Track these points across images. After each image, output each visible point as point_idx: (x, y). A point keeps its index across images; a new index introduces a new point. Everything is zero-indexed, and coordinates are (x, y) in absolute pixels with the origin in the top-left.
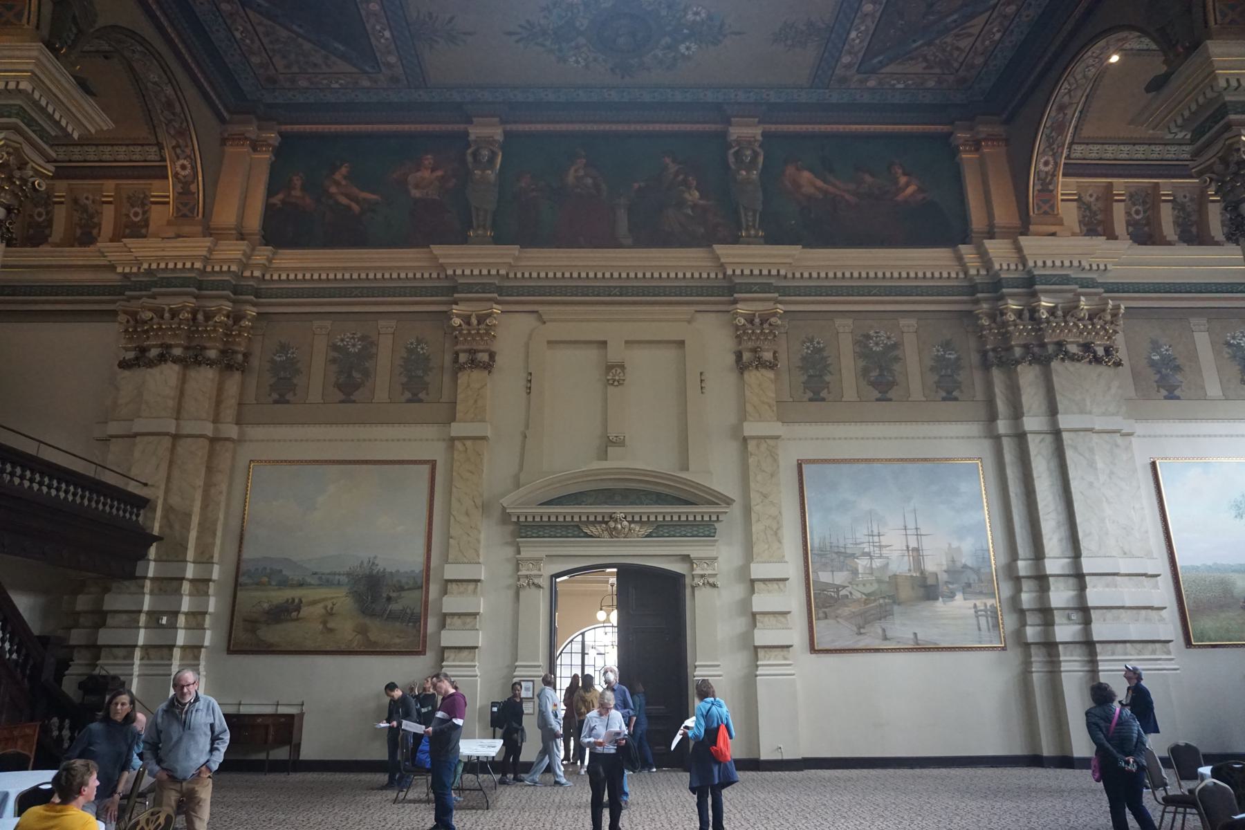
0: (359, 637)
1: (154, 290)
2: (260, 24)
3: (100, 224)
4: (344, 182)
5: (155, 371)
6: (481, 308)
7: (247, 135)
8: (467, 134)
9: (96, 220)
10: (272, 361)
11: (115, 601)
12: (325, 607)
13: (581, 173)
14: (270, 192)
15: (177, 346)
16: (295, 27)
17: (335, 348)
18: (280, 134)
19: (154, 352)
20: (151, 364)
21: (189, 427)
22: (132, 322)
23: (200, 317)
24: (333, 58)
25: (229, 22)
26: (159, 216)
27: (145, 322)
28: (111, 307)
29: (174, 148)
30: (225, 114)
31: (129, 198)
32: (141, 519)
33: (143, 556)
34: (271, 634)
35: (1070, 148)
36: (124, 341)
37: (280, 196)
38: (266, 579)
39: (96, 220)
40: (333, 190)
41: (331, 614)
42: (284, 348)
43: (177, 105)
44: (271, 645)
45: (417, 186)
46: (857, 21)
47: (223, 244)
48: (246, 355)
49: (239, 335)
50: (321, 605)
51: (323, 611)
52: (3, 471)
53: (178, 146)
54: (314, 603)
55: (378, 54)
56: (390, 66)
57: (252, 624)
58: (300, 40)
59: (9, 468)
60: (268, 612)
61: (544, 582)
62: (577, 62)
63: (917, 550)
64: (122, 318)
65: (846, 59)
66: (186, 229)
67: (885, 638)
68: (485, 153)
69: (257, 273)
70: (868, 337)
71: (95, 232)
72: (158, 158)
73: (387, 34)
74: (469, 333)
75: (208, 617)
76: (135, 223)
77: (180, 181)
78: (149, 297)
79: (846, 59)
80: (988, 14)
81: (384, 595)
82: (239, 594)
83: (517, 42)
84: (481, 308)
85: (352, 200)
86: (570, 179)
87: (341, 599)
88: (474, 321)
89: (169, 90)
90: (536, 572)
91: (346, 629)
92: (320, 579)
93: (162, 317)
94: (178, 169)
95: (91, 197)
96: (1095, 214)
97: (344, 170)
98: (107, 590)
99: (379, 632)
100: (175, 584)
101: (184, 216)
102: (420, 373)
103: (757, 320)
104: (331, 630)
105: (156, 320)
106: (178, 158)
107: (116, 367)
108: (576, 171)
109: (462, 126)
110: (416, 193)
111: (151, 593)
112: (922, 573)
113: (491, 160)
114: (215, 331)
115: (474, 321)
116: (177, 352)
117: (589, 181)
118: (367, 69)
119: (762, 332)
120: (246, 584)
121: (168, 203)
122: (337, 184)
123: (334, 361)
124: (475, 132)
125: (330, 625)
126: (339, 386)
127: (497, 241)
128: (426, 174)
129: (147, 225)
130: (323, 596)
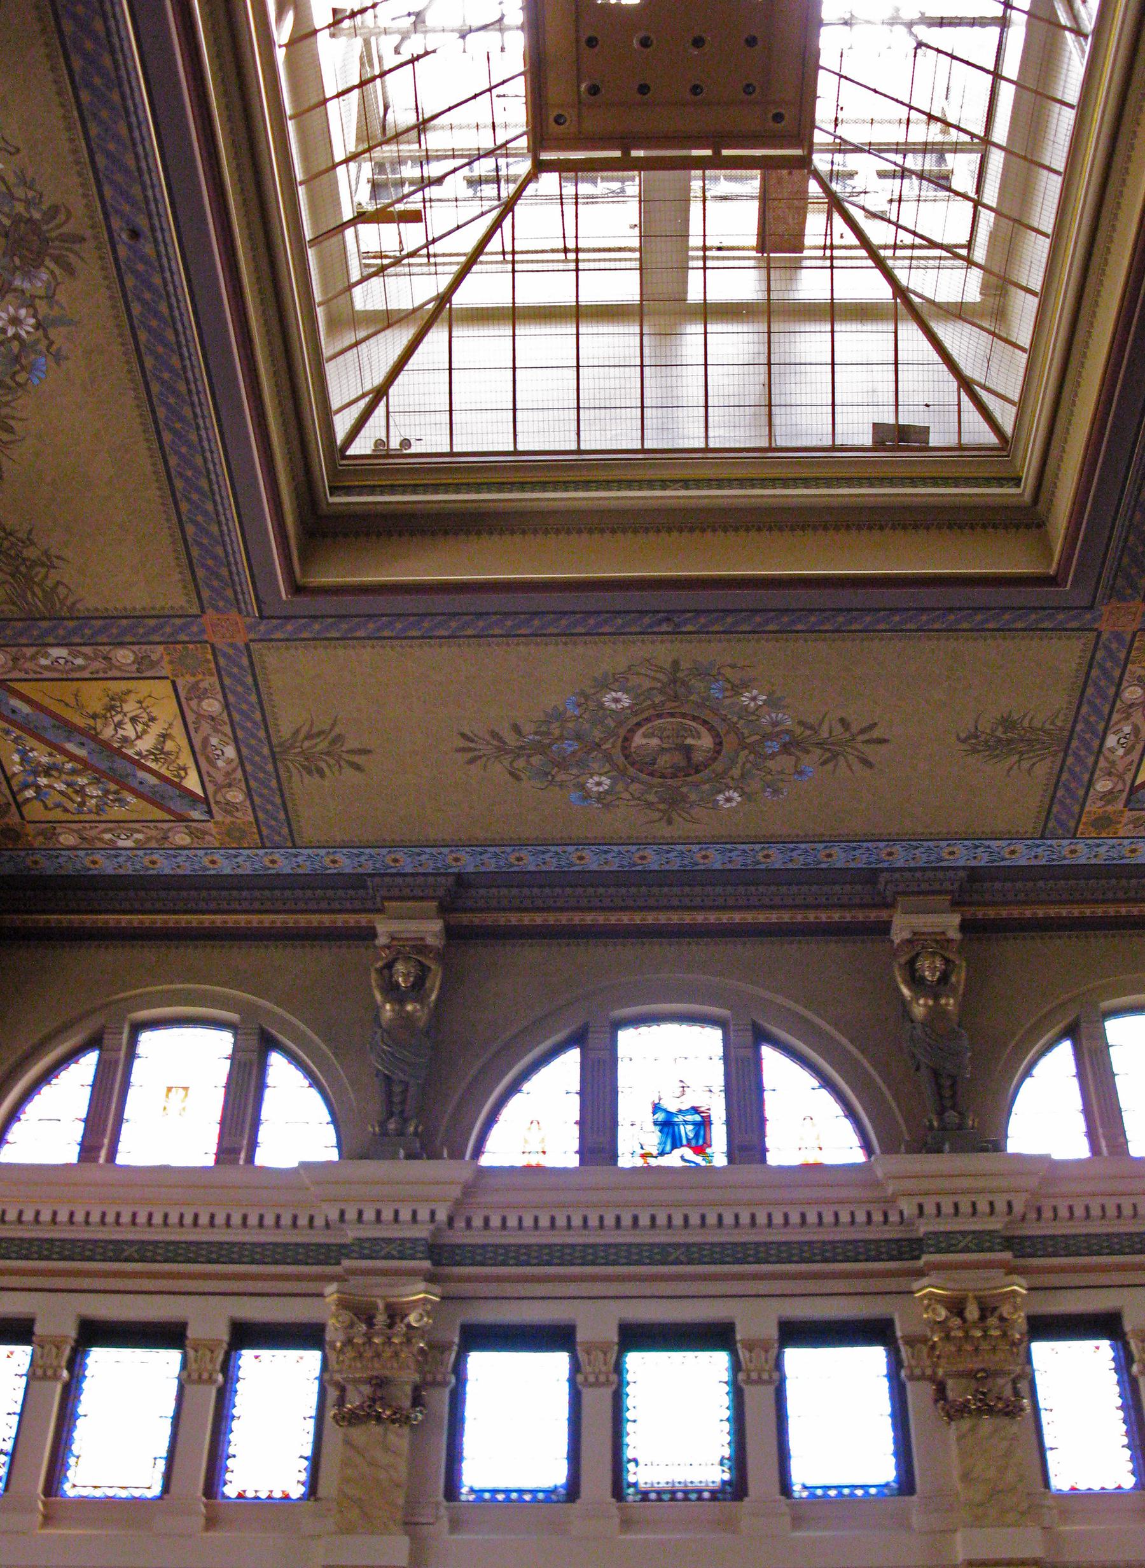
1: (346, 1263)
46: (1116, 717)
56: (230, 808)
65: (1103, 785)
73: (230, 752)
74: (967, 1337)
79: (1103, 785)
80: (11, 684)
115: (972, 1312)
119: (985, 1336)
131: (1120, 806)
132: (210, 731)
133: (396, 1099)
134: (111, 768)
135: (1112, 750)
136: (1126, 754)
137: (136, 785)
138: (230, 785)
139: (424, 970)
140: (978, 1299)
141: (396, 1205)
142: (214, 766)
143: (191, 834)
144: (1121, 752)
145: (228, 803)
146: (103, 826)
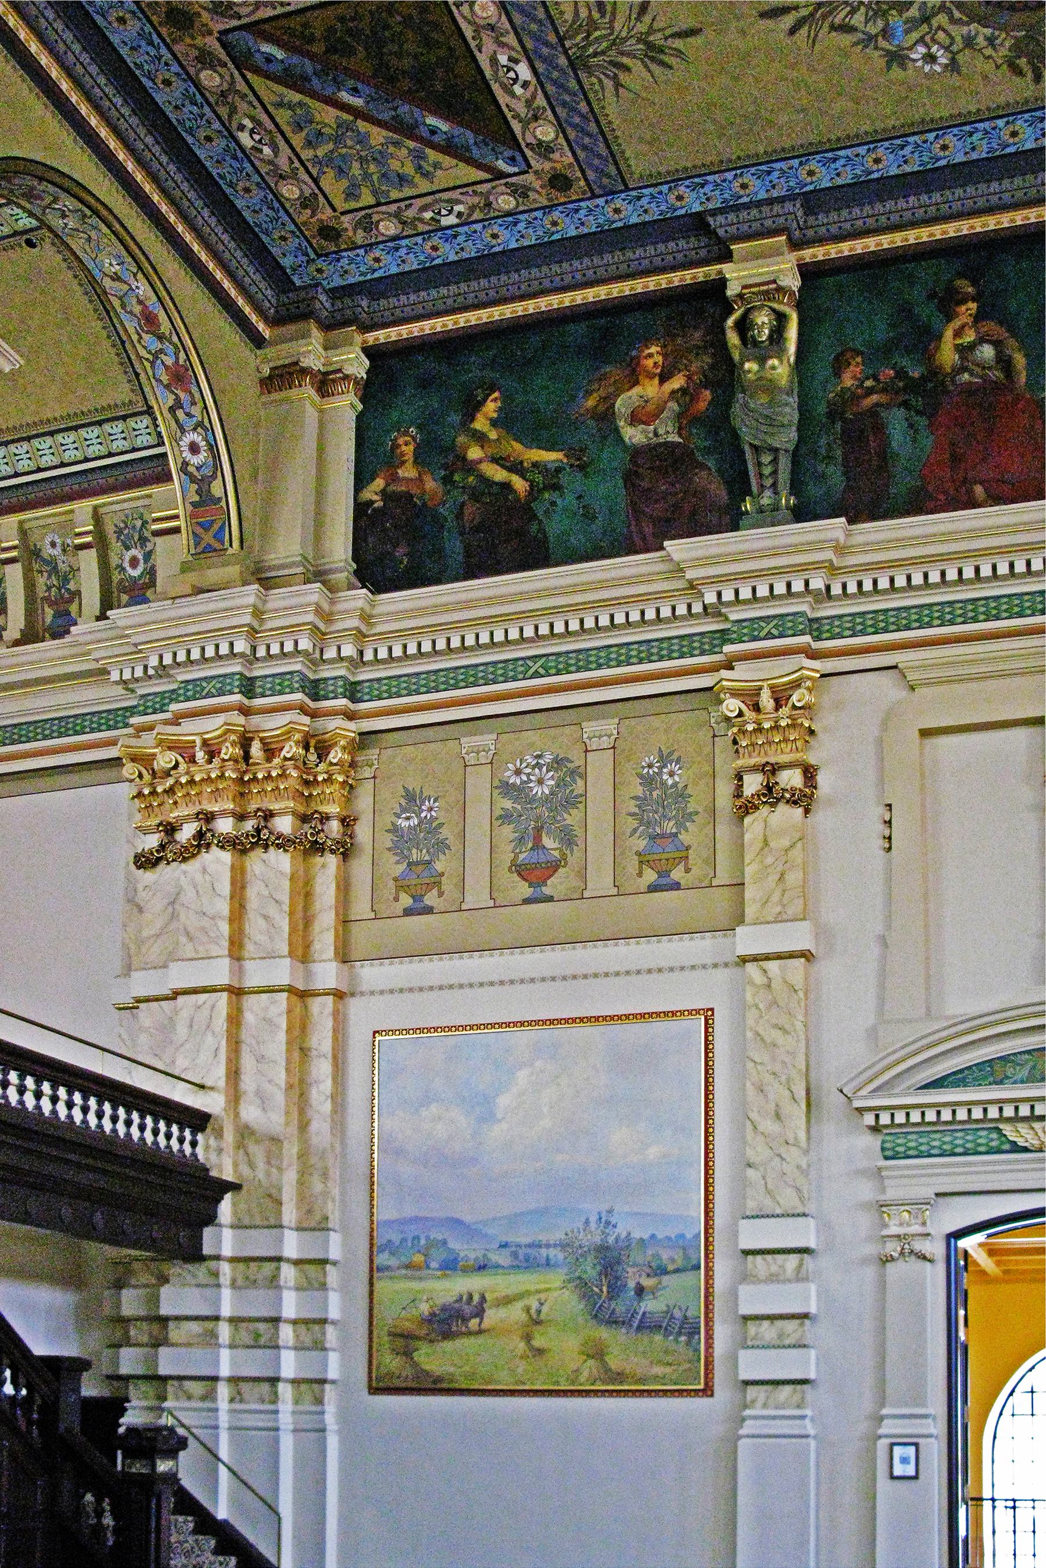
0: (591, 1362)
2: (280, 105)
3: (78, 593)
4: (493, 435)
5: (192, 867)
6: (779, 671)
7: (305, 363)
8: (722, 283)
9: (72, 586)
10: (395, 830)
11: (174, 1300)
12: (528, 1310)
13: (970, 337)
14: (361, 481)
15: (223, 813)
16: (345, 96)
17: (506, 789)
18: (367, 351)
19: (186, 833)
20: (186, 855)
21: (255, 975)
22: (147, 777)
23: (256, 750)
24: (432, 155)
25: (223, 111)
26: (170, 554)
27: (167, 774)
28: (112, 753)
29: (172, 410)
30: (261, 327)
31: (119, 532)
32: (199, 1150)
33: (210, 1219)
34: (434, 1358)
36: (138, 816)
37: (379, 483)
38: (419, 1258)
39: (72, 586)
40: (474, 453)
41: (538, 1323)
42: (412, 800)
43: (162, 316)
44: (439, 1379)
45: (635, 419)
47: (278, 598)
48: (347, 822)
49: (329, 780)
50: (520, 1305)
51: (524, 1317)
52: (5, 1084)
53: (178, 404)
54: (507, 1301)
55: (516, 127)
56: (544, 149)
57: (405, 1341)
58: (362, 126)
59: (13, 1077)
60: (430, 1319)
61: (936, 1248)
62: (931, 58)
64: (129, 769)
66: (214, 575)
68: (763, 319)
69: (348, 650)
71: (73, 608)
72: (152, 440)
75: (330, 1329)
76: (134, 580)
77: (193, 479)
78: (166, 722)
81: (632, 1284)
82: (378, 1286)
83: (792, 31)
84: (779, 671)
85: (510, 470)
86: (947, 355)
87: (556, 1292)
88: (766, 701)
89: (143, 288)
90: (916, 1229)
91: (566, 1349)
92: (515, 1255)
93: (192, 760)
94: (187, 455)
95: (58, 541)
97: (491, 407)
98: (164, 1280)
99: (624, 1351)
100: (268, 1268)
101: (209, 549)
102: (670, 827)
104: (540, 1352)
105: (183, 767)
106: (183, 431)
107: (133, 867)
108: (958, 334)
109: (711, 271)
110: (634, 435)
111: (234, 1285)
113: (778, 334)
114: (283, 775)
115: (766, 701)
116: (225, 826)
117: (987, 352)
118: (501, 165)
120: (388, 1268)
121: (176, 530)
122: (480, 438)
123: (506, 817)
124: (736, 276)
125: (538, 1342)
126: (522, 871)
127: (801, 514)
128: (650, 389)
129: (152, 583)
130: (522, 1288)
131: (530, 178)
132: (494, 47)
133: (767, 471)
134: (393, 118)
136: (458, 202)
137: (425, 134)
138: (536, 118)
139: (781, 318)
140: (772, 687)
141: (787, 578)
142: (513, 95)
143: (513, 193)
145: (540, 143)
146: (419, 203)
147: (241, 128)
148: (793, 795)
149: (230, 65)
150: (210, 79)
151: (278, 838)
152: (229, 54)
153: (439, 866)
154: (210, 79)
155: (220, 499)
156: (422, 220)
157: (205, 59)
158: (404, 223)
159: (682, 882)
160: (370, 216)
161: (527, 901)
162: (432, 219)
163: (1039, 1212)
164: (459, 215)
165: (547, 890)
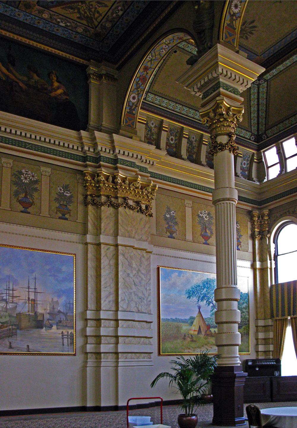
35: (146, 94)
63: (34, 300)
67: (11, 347)
70: (21, 173)
96: (193, 148)
103: (127, 182)
112: (36, 313)
135: (121, 10)
136: (118, 7)
144: (120, 8)
147: (59, 22)
148: (117, 205)
149: (46, 10)
150: (45, 16)
151: (99, 203)
152: (44, 8)
153: (70, 208)
154: (45, 16)
155: (135, 114)
156: (114, 18)
157: (40, 12)
158: (111, 21)
159: (175, 238)
160: (102, 25)
161: (22, 212)
162: (116, 15)
163: (1, 294)
164: (121, 10)
165: (29, 210)
